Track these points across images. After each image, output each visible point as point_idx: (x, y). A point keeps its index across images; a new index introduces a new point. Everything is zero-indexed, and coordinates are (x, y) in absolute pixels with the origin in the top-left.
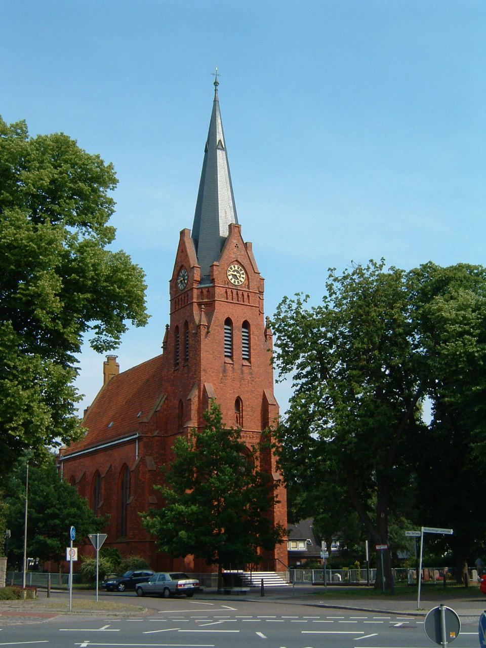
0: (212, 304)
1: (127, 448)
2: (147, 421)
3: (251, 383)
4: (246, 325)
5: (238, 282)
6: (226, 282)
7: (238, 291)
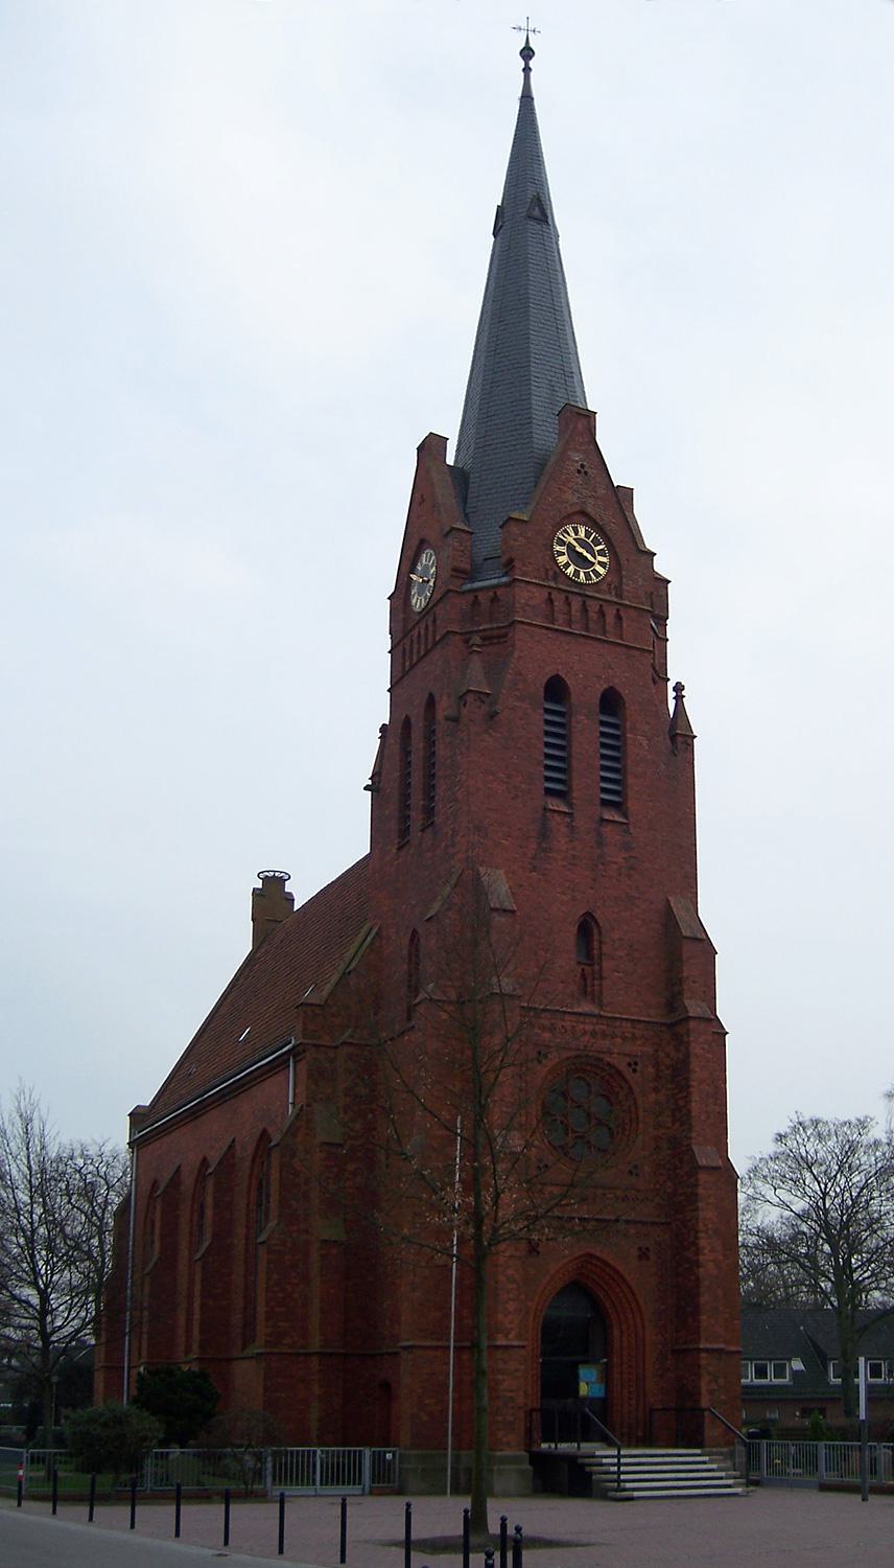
0: (506, 635)
1: (270, 1086)
2: (318, 1002)
3: (629, 876)
4: (611, 702)
5: (587, 575)
6: (551, 573)
7: (589, 602)
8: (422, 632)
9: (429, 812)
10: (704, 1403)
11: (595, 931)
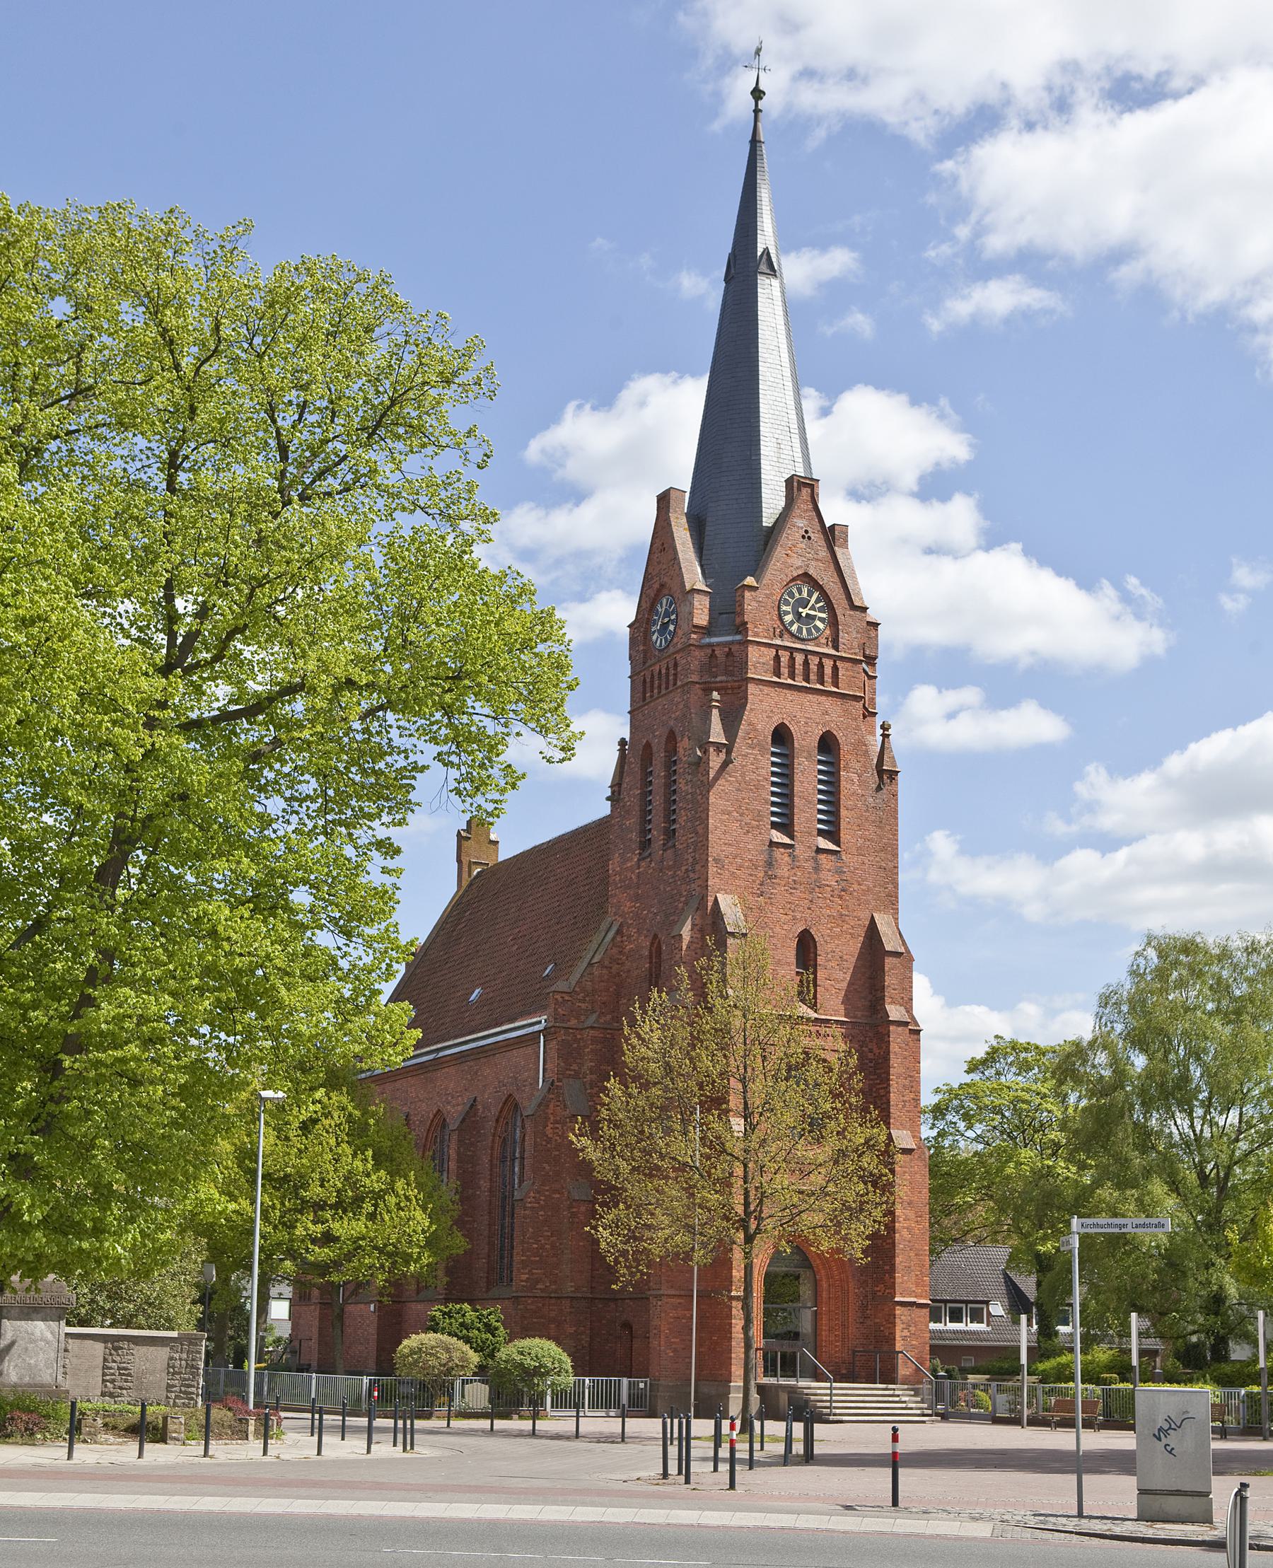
3: (840, 897)
4: (828, 744)
5: (809, 631)
8: (664, 671)
9: (670, 834)
10: (898, 1347)
11: (811, 945)
